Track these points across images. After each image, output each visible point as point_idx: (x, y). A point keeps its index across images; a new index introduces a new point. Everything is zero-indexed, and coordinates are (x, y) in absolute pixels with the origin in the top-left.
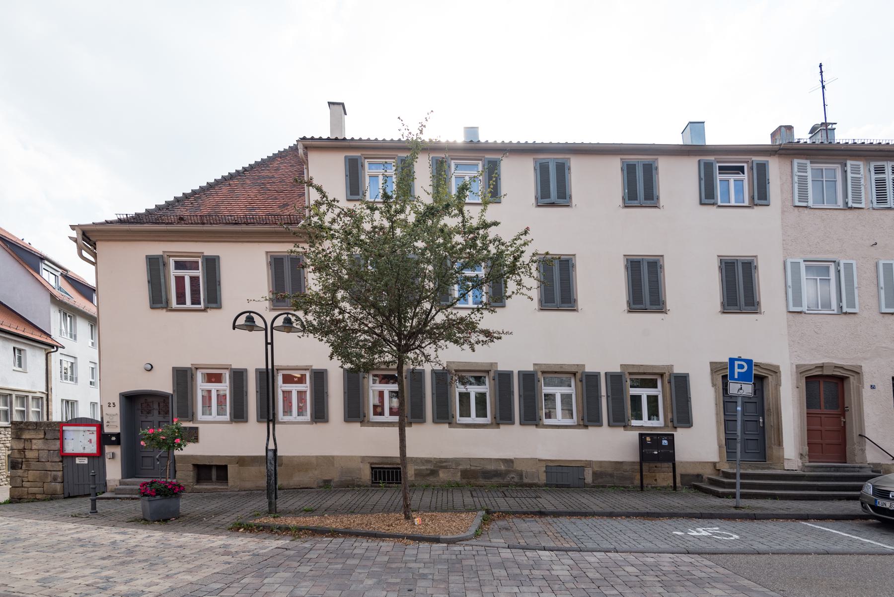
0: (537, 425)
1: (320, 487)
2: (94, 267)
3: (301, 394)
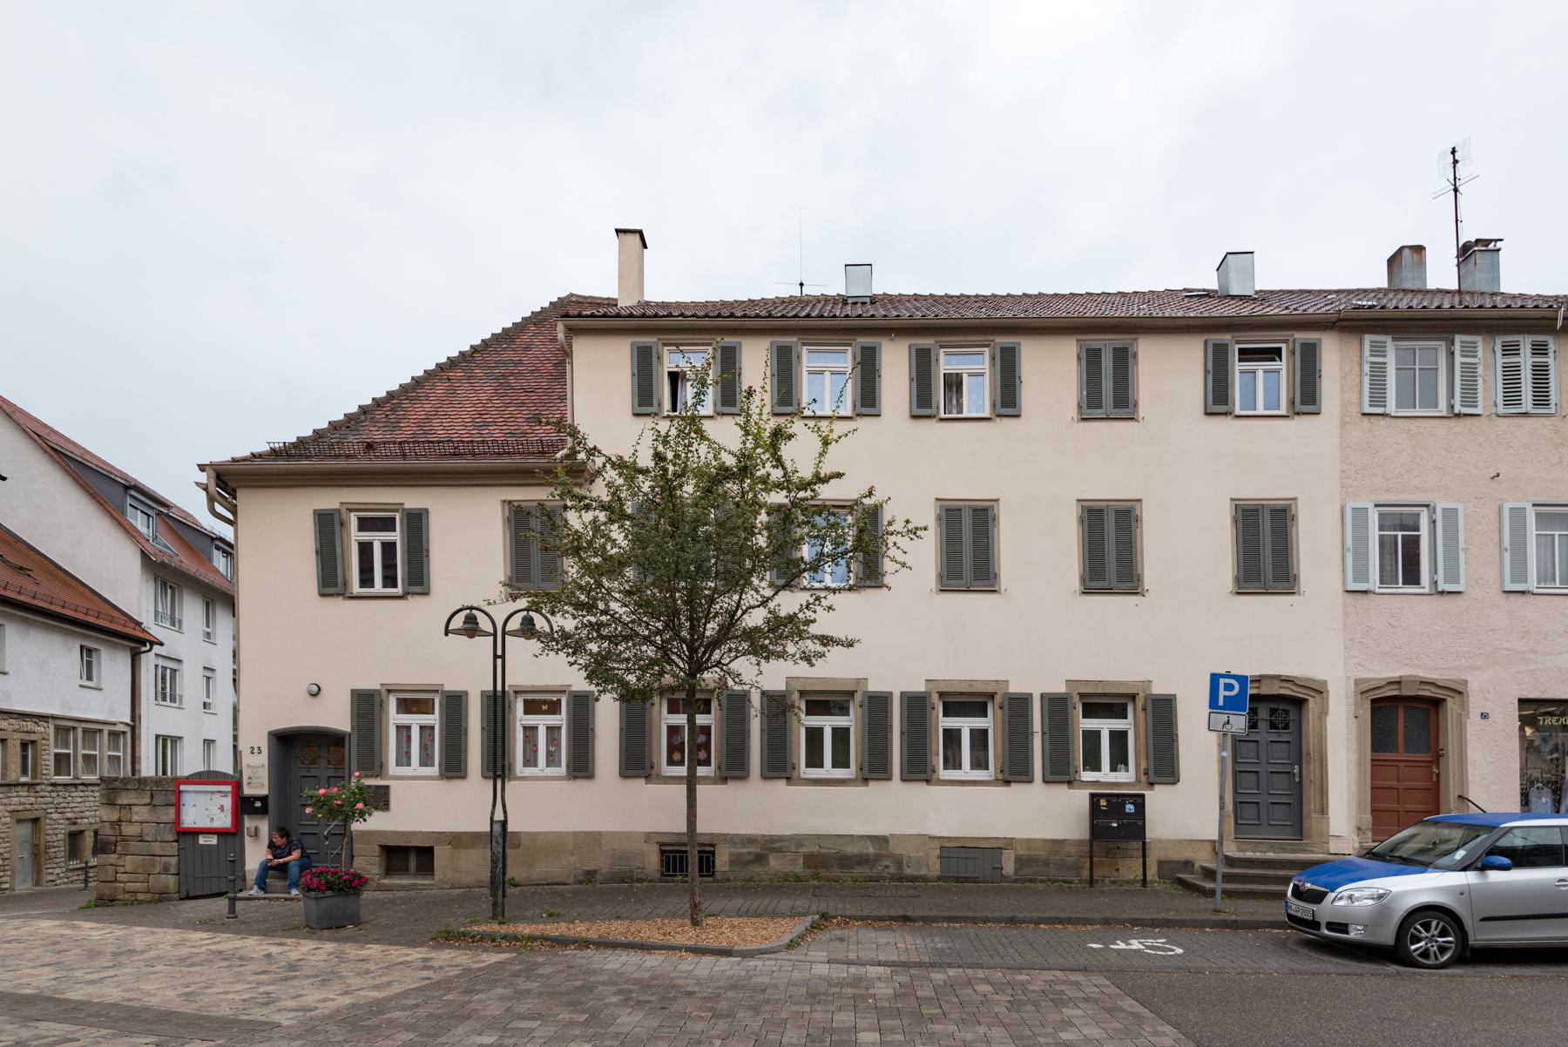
0: (928, 781)
1: (580, 882)
2: (231, 528)
3: (553, 731)
